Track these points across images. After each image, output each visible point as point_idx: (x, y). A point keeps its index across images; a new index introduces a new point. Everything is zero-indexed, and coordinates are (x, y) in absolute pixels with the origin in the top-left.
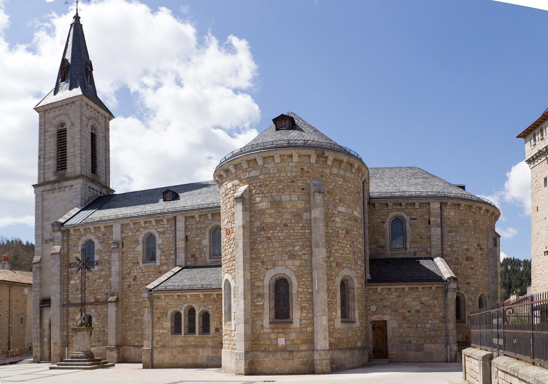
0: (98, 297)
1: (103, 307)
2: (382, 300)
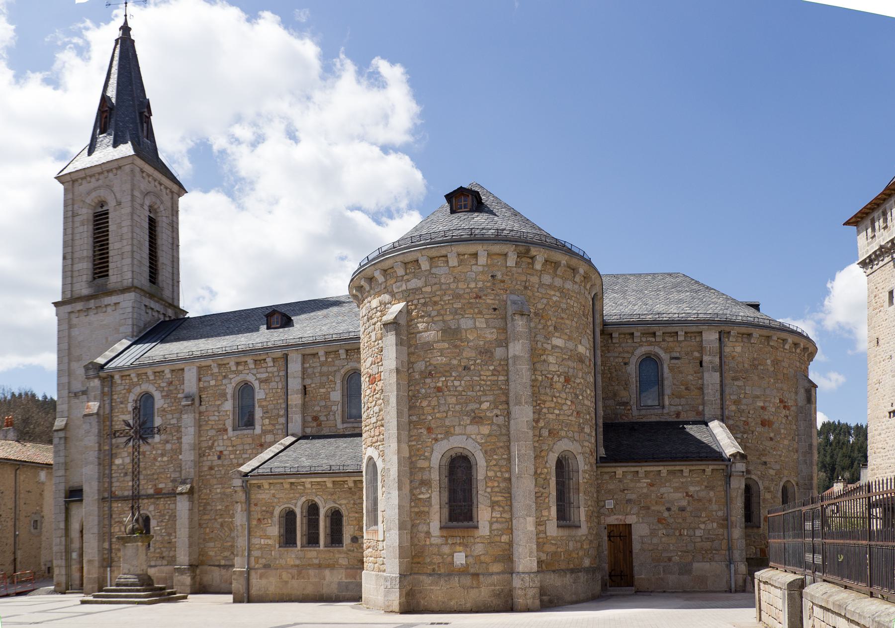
0: (161, 486)
1: (169, 502)
2: (624, 490)
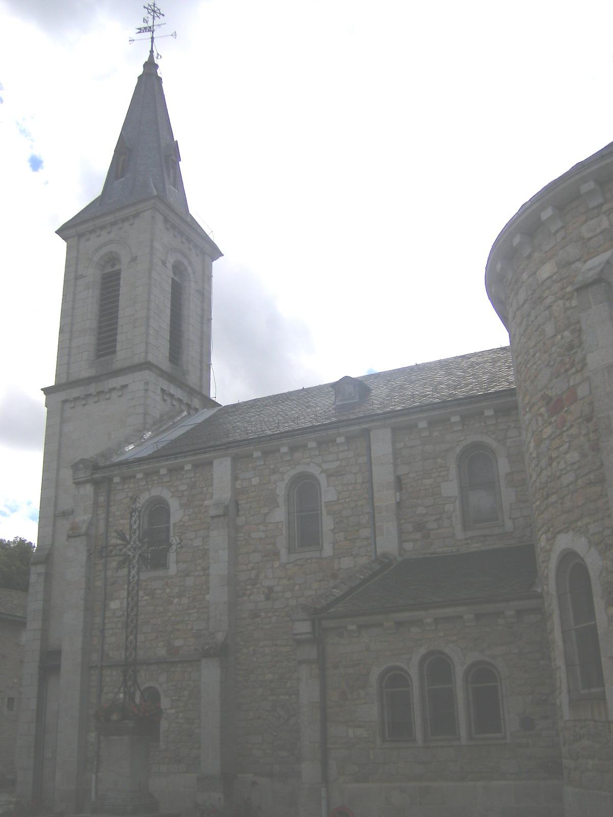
0: (178, 643)
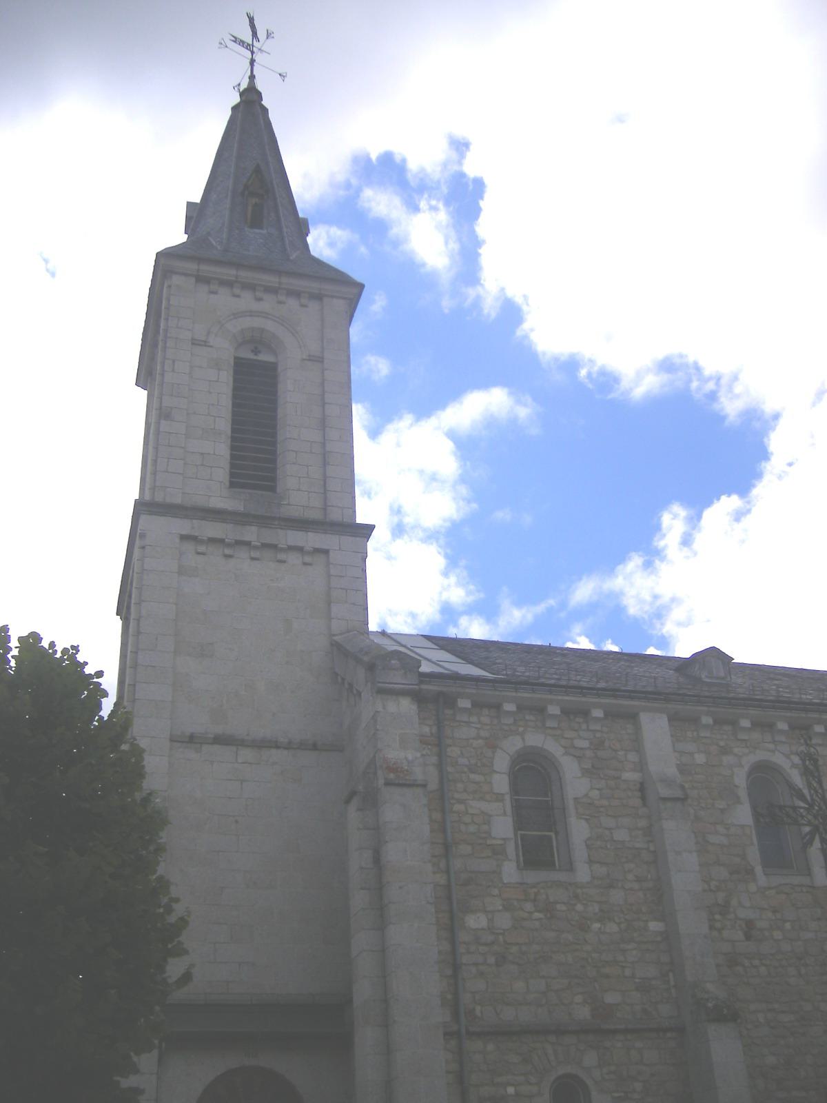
0: (611, 998)
